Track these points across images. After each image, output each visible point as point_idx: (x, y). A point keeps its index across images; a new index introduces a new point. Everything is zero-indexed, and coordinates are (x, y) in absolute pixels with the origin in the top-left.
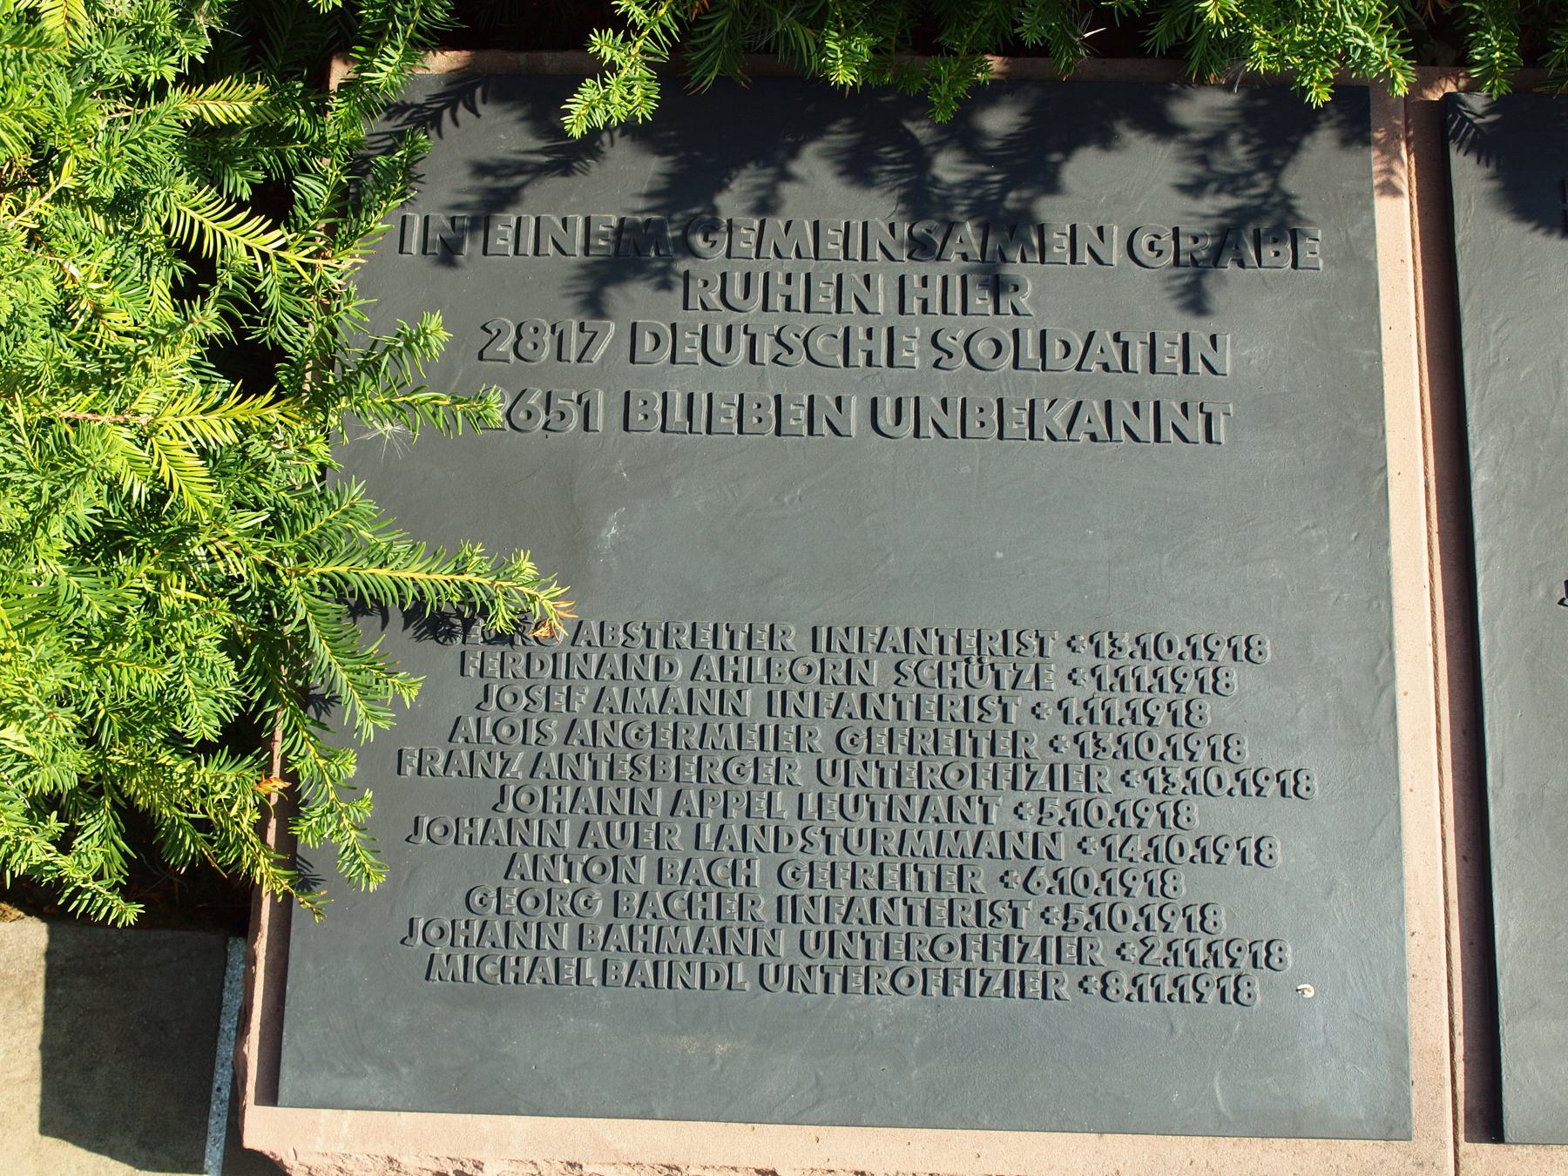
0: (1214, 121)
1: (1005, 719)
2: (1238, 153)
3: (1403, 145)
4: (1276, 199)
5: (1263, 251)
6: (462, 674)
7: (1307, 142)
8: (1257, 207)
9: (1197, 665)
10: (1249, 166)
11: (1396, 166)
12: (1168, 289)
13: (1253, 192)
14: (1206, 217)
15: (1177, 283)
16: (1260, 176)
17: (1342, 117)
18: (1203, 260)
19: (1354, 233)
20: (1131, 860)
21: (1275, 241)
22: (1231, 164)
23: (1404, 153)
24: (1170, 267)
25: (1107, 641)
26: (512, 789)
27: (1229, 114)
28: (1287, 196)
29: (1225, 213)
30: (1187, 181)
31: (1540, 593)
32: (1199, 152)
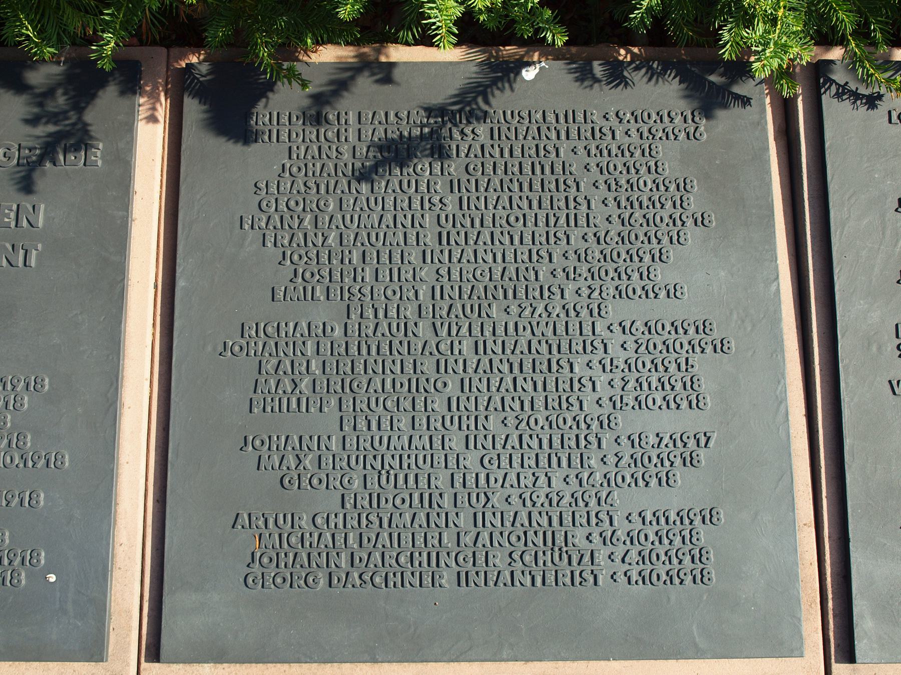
0: (47, 81)
2: (61, 100)
3: (162, 94)
4: (79, 126)
5: (67, 156)
6: (251, 412)
7: (100, 93)
8: (68, 131)
10: (66, 108)
11: (158, 106)
12: (12, 179)
13: (67, 122)
14: (38, 137)
15: (18, 175)
16: (72, 113)
17: (122, 78)
18: (33, 162)
19: (121, 145)
21: (76, 150)
22: (56, 107)
23: (163, 99)
24: (14, 167)
27: (58, 77)
28: (86, 125)
29: (50, 135)
30: (29, 117)
31: (209, 348)
32: (39, 100)
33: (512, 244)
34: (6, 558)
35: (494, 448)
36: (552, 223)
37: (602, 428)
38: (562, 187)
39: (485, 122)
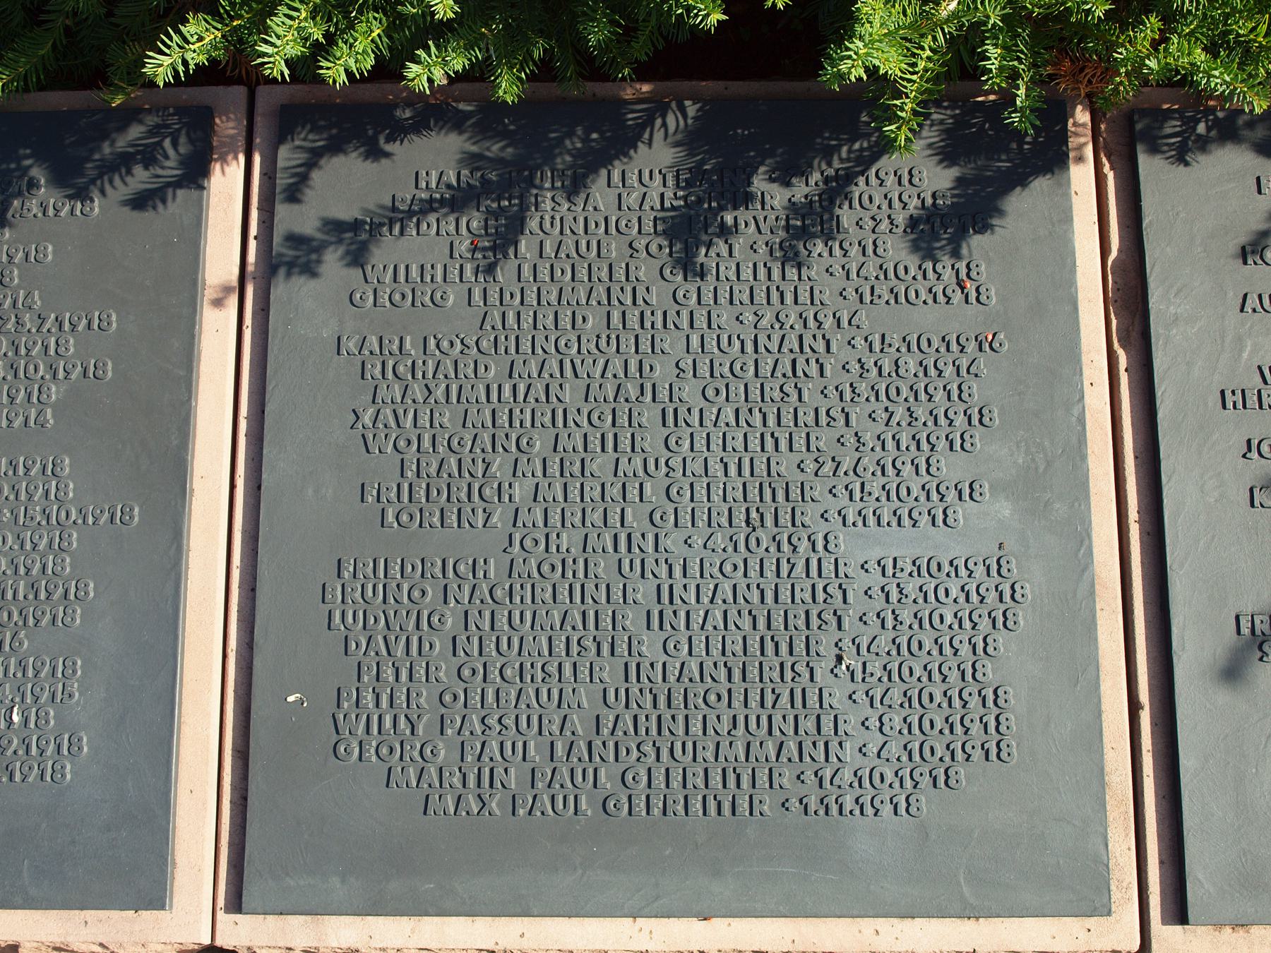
1: (812, 679)
9: (930, 505)
20: (890, 707)
25: (848, 389)
26: (426, 613)
33: (740, 475)
34: (31, 618)
35: (701, 425)
36: (784, 573)
37: (988, 575)
38: (789, 675)
39: (747, 208)
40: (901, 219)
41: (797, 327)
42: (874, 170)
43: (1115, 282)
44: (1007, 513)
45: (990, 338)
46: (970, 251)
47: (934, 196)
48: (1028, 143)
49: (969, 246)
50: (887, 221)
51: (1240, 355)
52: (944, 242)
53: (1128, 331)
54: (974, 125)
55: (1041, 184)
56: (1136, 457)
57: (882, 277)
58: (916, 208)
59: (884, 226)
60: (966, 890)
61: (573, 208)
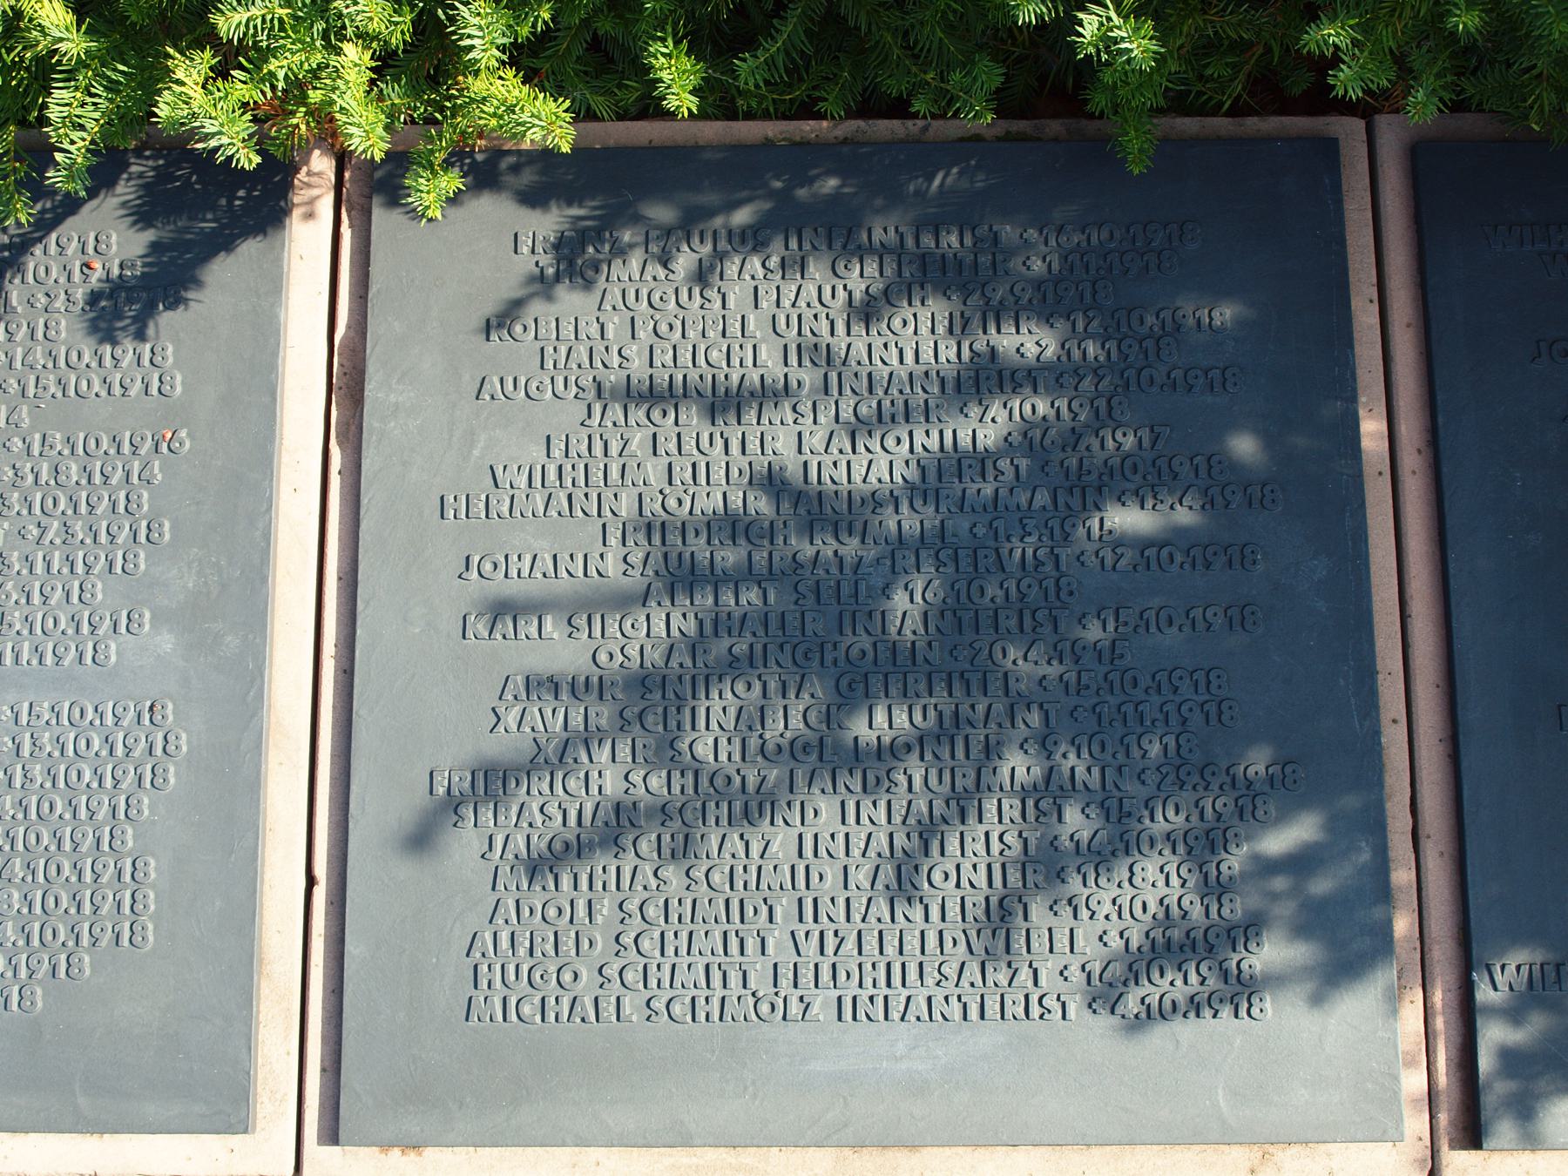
40: (80, 295)
41: (999, 419)
42: (54, 236)
43: (341, 365)
44: (168, 647)
45: (169, 435)
46: (157, 332)
47: (121, 266)
48: (240, 198)
49: (157, 325)
50: (63, 296)
51: (470, 452)
52: (128, 321)
53: (348, 424)
54: (178, 178)
55: (249, 248)
56: (340, 579)
57: (50, 365)
58: (100, 280)
59: (59, 304)
60: (82, 1101)
61: (671, 276)
